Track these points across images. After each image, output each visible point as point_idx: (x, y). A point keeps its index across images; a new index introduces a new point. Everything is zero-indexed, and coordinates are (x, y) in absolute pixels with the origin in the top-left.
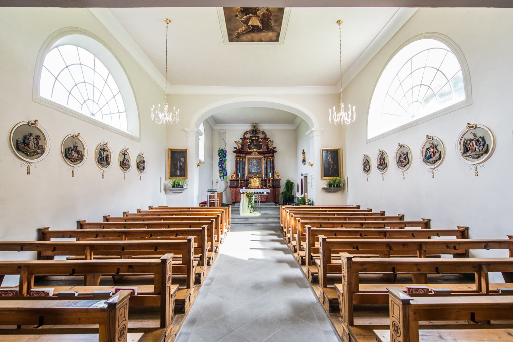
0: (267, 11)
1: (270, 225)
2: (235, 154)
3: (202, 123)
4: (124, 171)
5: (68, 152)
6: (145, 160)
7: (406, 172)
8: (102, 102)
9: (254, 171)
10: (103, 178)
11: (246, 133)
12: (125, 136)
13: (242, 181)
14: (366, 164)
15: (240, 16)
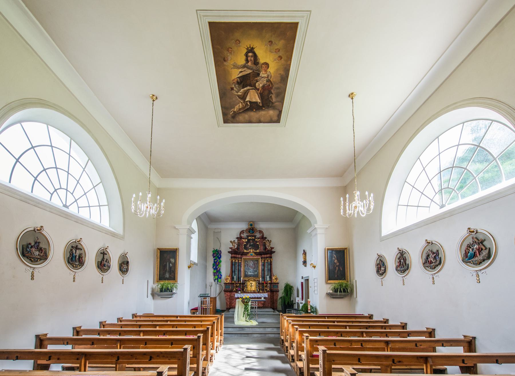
0: (268, 82)
1: (268, 336)
3: (195, 220)
4: (122, 275)
5: (26, 249)
6: (129, 261)
7: (436, 275)
8: (79, 193)
10: (74, 281)
11: (242, 232)
12: (104, 232)
13: (237, 284)
14: (380, 266)
15: (236, 90)
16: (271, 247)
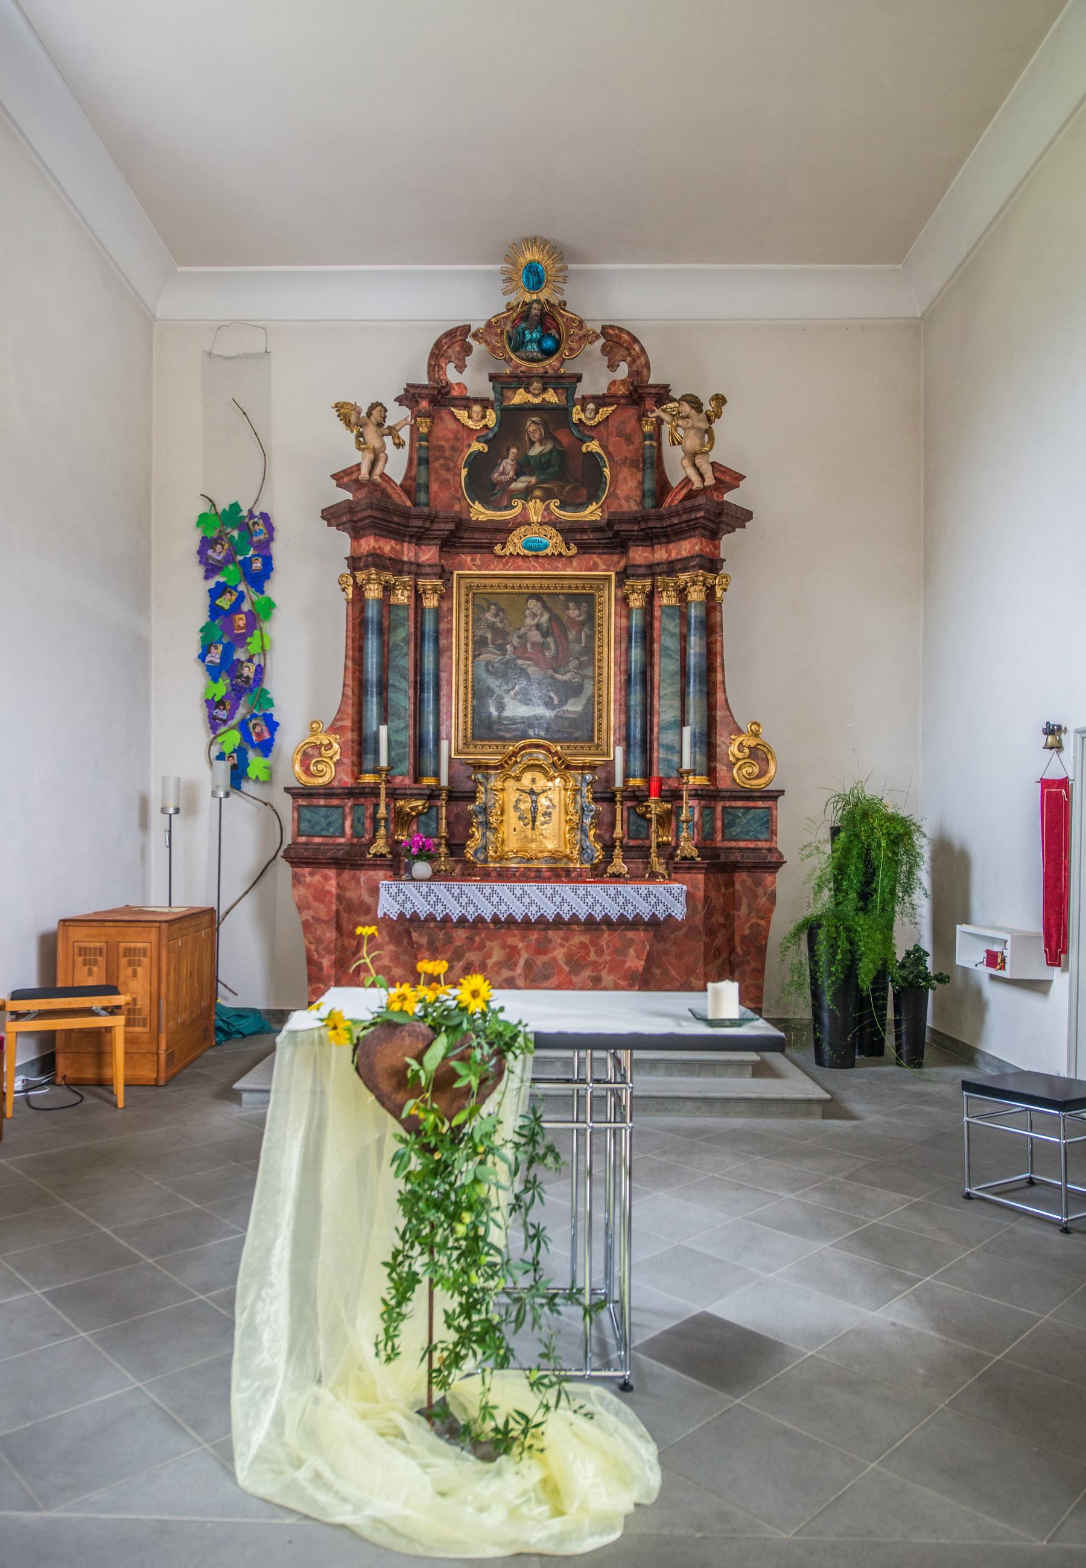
2: (342, 543)
13: (404, 796)
16: (714, 465)
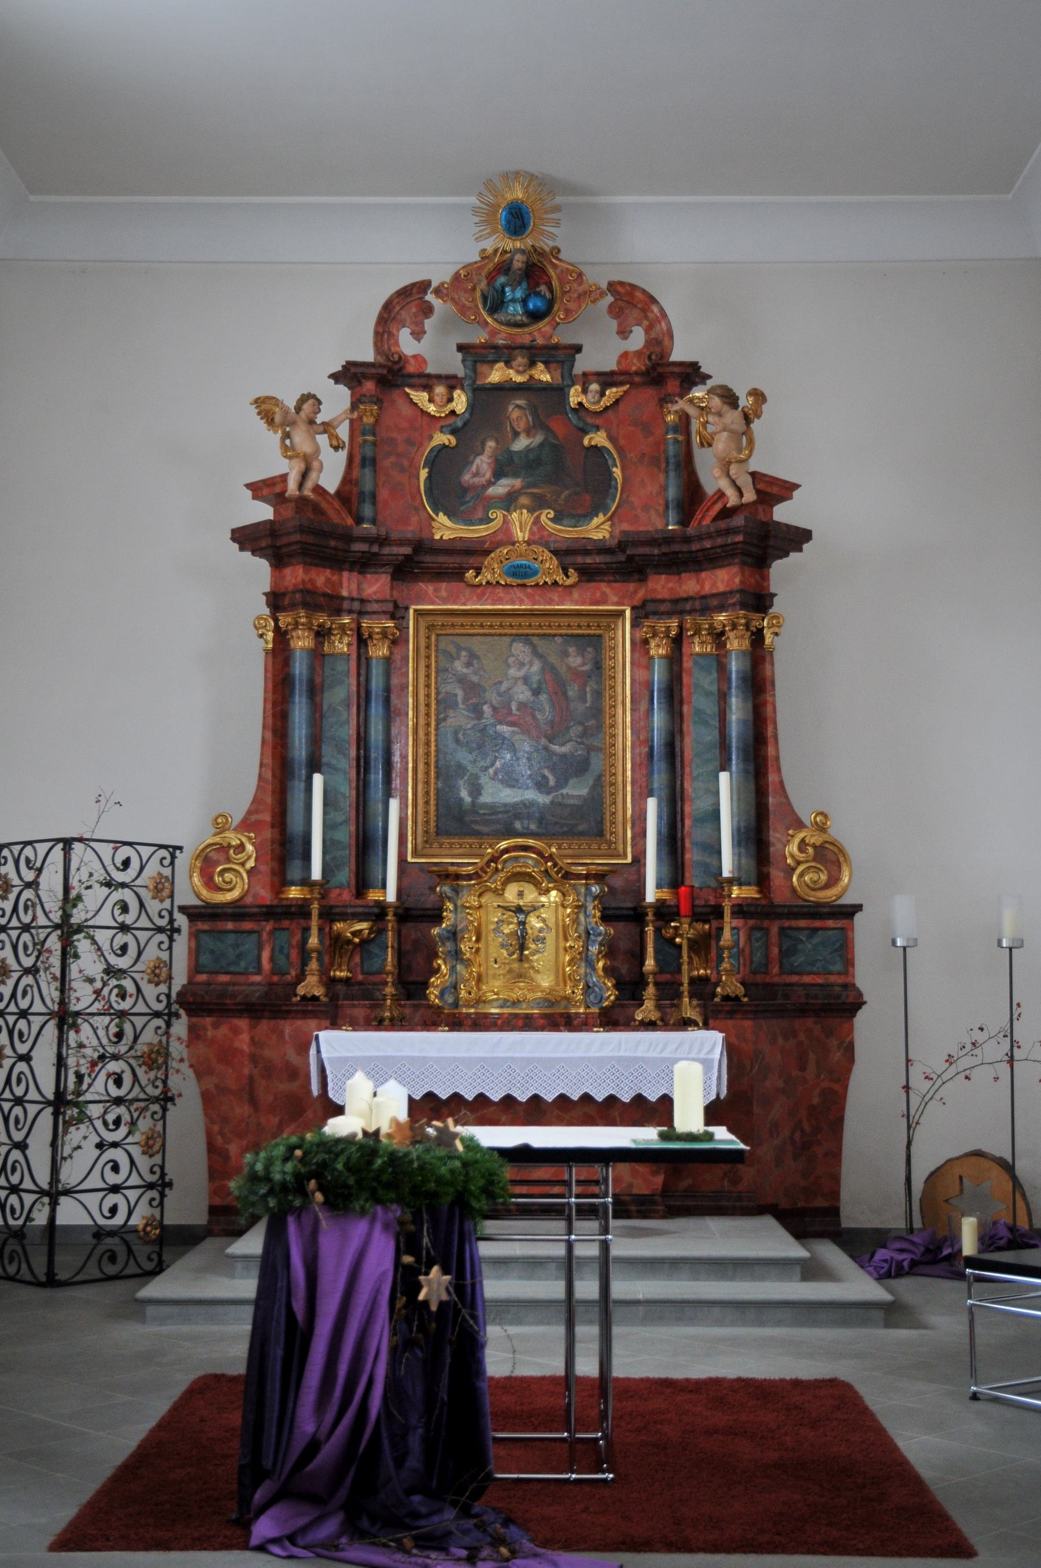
9: (507, 796)
13: (344, 917)
